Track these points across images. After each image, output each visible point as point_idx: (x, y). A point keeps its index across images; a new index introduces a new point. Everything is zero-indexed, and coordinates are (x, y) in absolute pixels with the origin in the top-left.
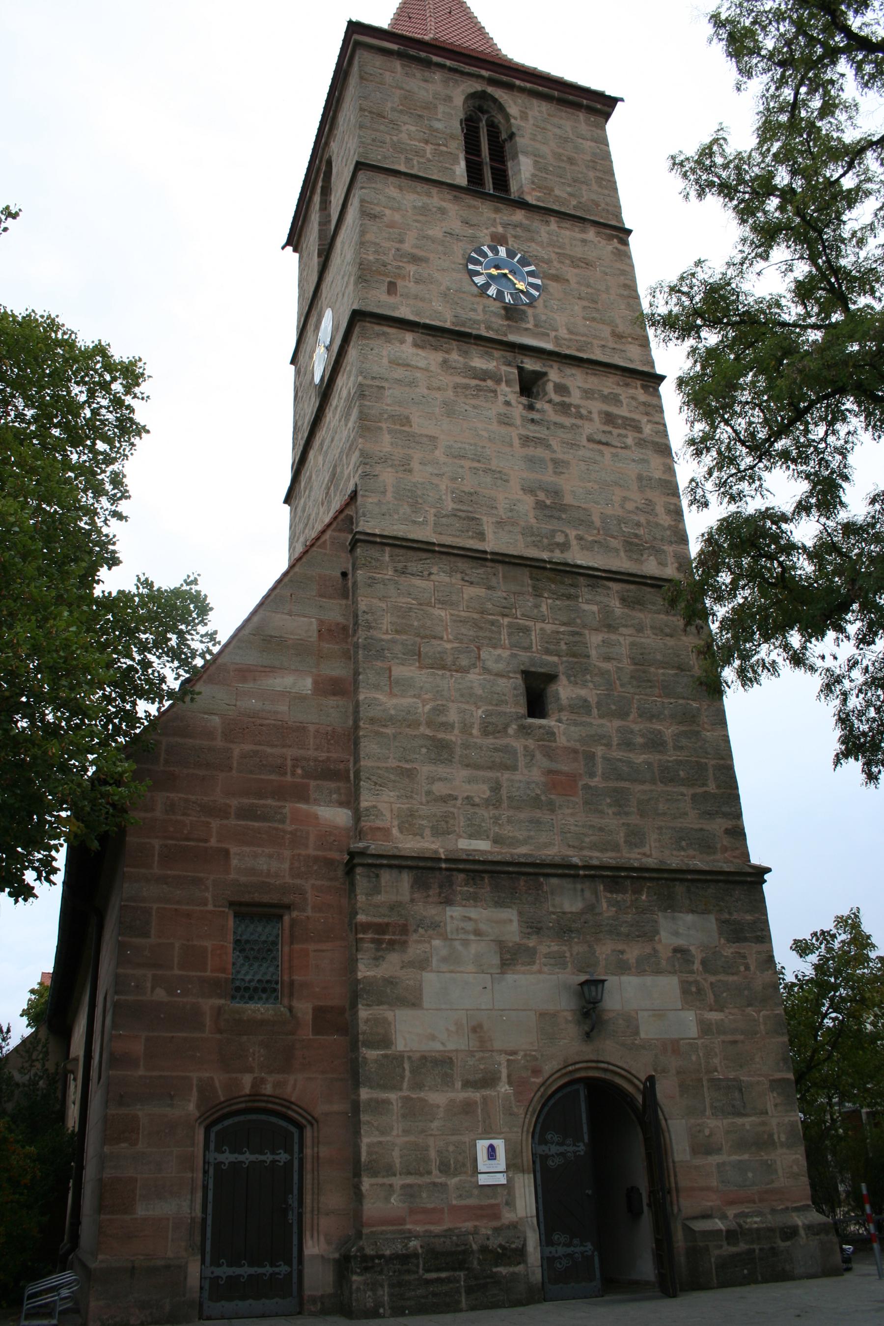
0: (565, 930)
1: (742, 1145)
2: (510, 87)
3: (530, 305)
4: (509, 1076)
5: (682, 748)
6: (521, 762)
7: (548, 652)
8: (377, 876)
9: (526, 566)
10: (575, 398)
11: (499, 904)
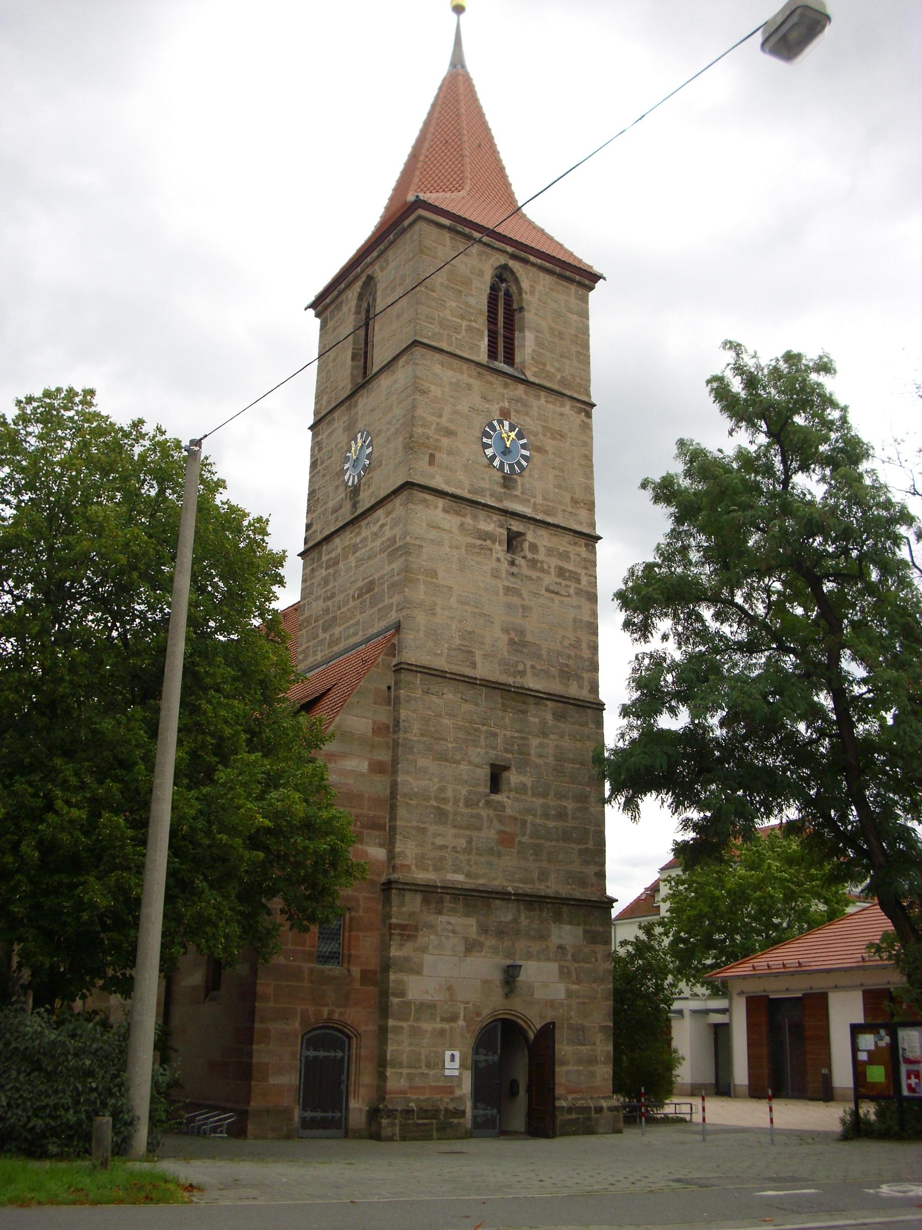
0: (501, 933)
1: (579, 1062)
2: (525, 261)
3: (520, 475)
4: (464, 1016)
5: (576, 818)
6: (485, 824)
7: (506, 751)
8: (404, 895)
9: (499, 689)
10: (541, 556)
11: (467, 915)
